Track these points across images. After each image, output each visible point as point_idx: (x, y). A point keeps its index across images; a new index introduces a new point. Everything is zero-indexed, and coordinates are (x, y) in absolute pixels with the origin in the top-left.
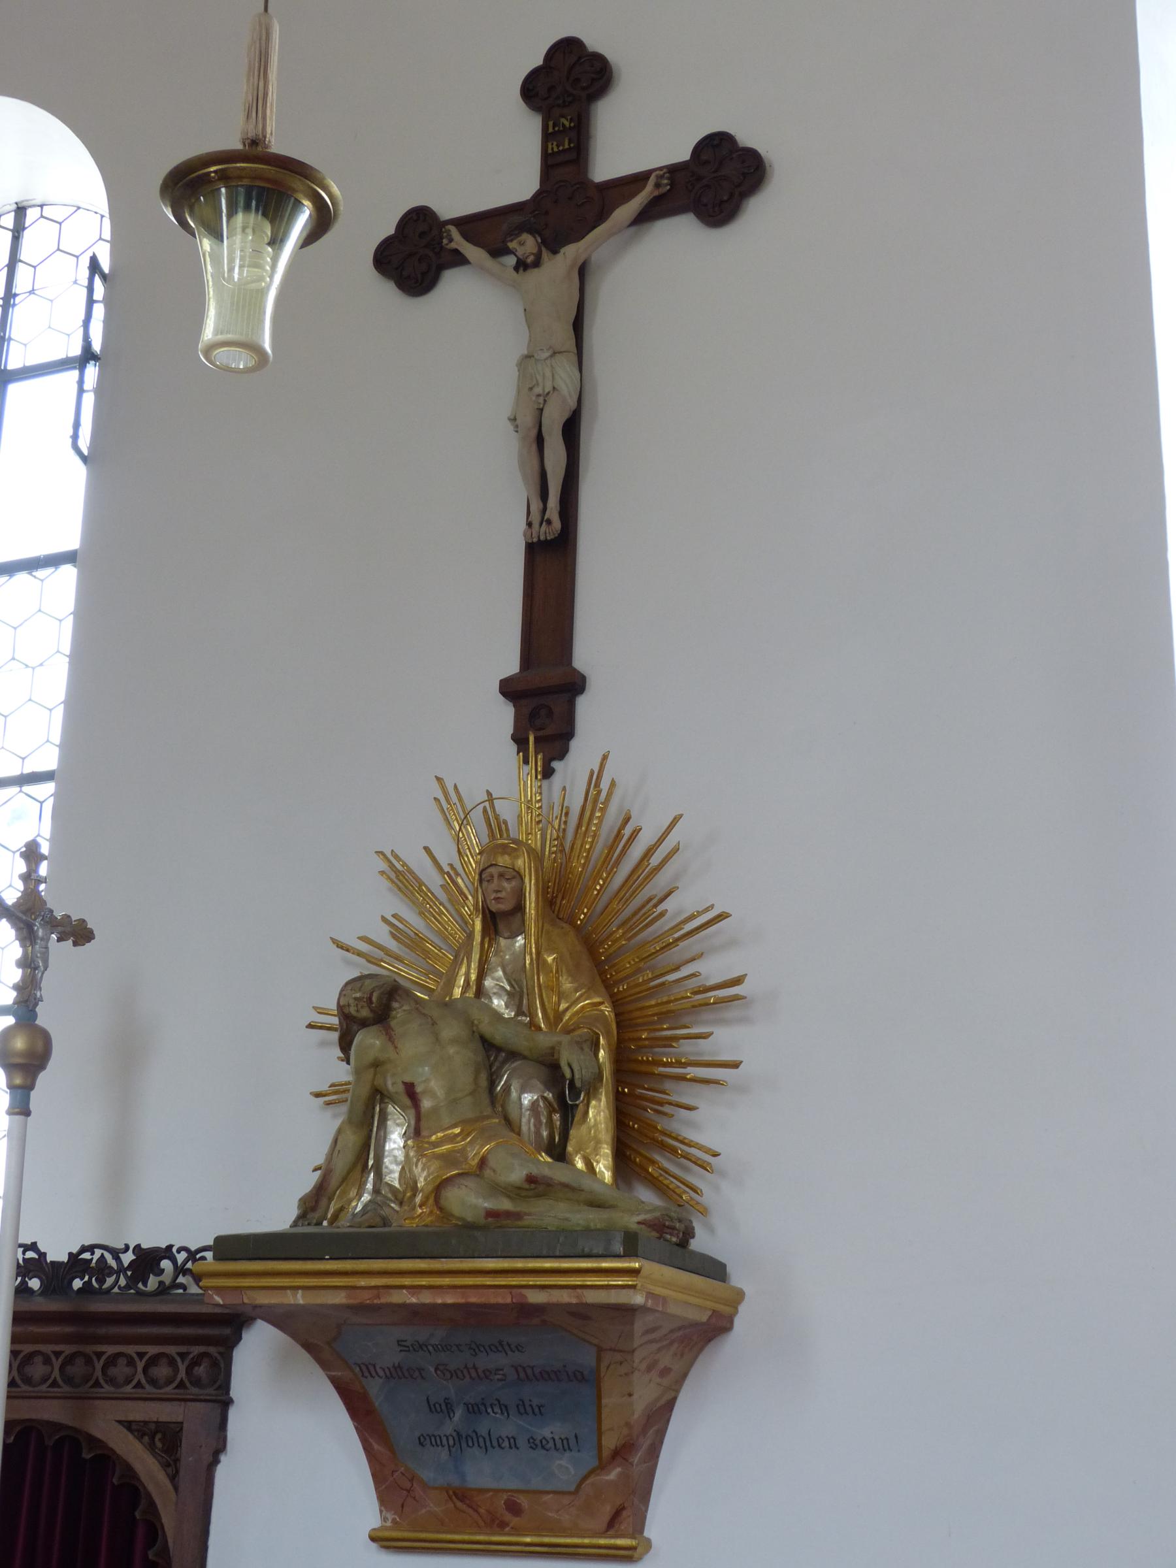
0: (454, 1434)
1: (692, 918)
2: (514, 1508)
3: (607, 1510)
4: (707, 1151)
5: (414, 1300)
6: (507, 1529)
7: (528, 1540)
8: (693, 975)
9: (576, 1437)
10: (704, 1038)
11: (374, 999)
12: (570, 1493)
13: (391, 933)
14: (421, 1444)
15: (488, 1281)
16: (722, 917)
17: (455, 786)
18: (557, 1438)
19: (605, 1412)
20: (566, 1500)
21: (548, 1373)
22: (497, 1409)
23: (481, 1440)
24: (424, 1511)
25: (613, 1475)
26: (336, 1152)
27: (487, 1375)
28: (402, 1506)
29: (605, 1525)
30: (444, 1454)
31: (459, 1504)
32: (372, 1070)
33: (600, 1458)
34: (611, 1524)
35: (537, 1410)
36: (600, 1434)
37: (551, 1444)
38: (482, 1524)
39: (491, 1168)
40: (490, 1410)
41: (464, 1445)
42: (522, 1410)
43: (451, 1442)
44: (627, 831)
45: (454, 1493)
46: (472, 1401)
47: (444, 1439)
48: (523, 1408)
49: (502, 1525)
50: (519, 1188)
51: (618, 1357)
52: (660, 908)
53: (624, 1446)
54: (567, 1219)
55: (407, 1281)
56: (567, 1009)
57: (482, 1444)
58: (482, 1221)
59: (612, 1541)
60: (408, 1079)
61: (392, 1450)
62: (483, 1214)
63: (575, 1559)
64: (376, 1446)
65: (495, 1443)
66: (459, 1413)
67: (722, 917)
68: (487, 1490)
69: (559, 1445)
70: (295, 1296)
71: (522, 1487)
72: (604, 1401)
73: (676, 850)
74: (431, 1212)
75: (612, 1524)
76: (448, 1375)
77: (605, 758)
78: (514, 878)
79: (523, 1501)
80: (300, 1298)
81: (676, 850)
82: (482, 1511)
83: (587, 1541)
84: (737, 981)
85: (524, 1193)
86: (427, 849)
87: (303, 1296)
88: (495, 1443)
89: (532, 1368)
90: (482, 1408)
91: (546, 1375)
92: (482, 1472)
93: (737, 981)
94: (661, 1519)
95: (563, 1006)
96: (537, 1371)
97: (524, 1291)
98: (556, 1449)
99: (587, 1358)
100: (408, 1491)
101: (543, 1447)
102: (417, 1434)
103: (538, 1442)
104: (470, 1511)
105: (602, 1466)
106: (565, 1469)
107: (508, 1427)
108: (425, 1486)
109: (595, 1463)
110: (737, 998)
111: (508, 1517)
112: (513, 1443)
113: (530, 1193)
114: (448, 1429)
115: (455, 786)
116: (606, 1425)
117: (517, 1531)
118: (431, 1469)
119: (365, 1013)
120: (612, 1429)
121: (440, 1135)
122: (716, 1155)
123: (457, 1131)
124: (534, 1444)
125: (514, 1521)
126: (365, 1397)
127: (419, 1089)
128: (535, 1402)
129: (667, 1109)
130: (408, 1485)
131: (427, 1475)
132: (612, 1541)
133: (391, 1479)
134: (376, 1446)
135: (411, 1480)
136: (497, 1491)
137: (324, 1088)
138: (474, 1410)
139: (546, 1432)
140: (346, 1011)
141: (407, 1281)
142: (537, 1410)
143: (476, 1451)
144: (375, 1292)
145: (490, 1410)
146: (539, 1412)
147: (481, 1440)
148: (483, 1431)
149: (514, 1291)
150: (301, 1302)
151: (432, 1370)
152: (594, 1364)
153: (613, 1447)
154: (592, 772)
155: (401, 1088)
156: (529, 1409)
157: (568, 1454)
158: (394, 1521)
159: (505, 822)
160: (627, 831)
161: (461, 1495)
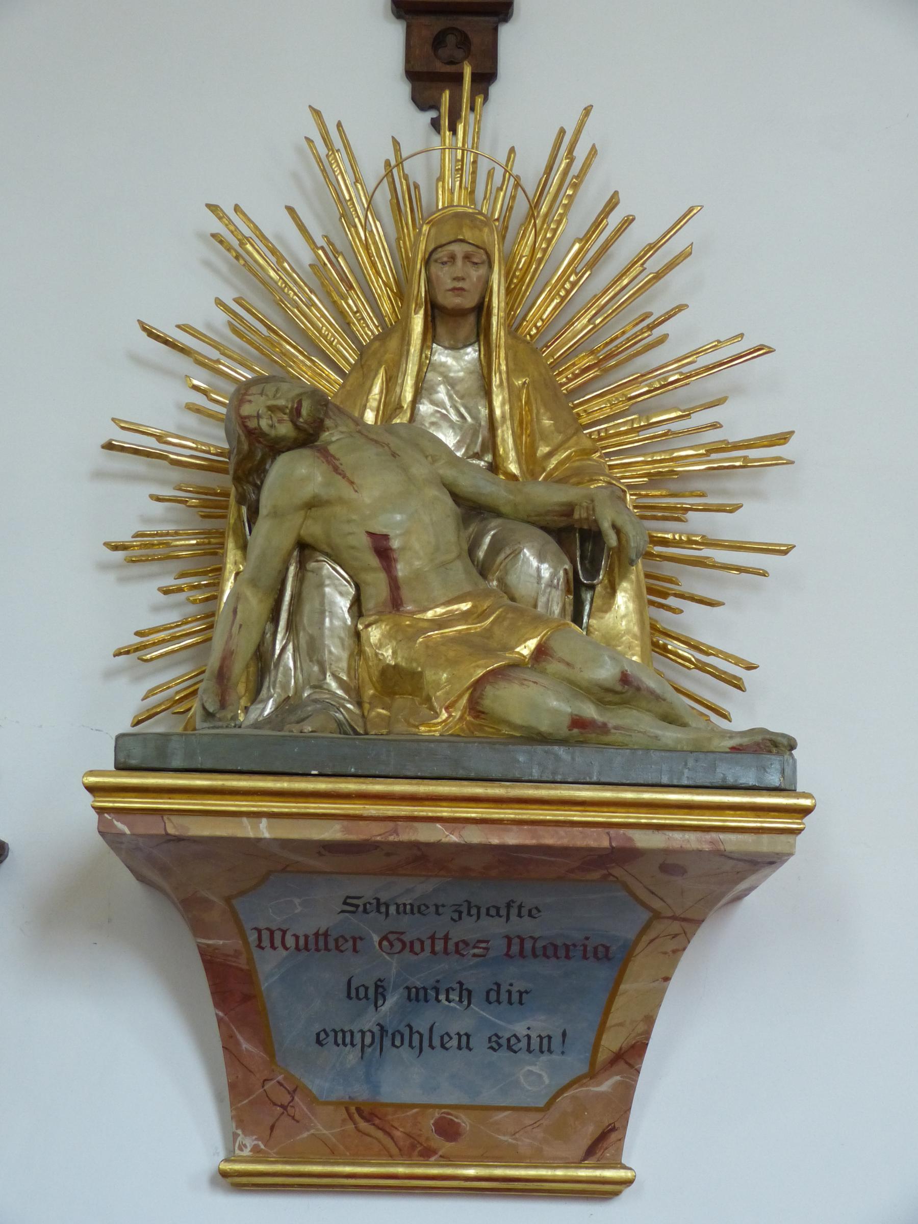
0: (376, 1029)
1: (718, 345)
2: (448, 1130)
3: (590, 1131)
4: (738, 661)
5: (454, 838)
6: (433, 1159)
7: (471, 1172)
8: (715, 426)
9: (564, 1034)
10: (731, 512)
11: (304, 412)
12: (537, 1110)
13: (230, 324)
14: (319, 1042)
15: (576, 816)
16: (762, 350)
17: (339, 125)
18: (534, 1035)
19: (619, 1001)
20: (528, 1119)
21: (556, 947)
22: (454, 996)
23: (416, 1037)
24: (305, 1135)
25: (606, 1086)
26: (236, 626)
27: (460, 948)
28: (272, 1128)
29: (581, 1152)
30: (352, 1056)
31: (363, 1125)
32: (302, 513)
33: (592, 1063)
34: (590, 1152)
35: (515, 997)
36: (602, 1028)
37: (524, 1044)
38: (394, 1150)
39: (561, 660)
40: (442, 997)
41: (387, 1042)
42: (493, 996)
43: (368, 1040)
44: (614, 220)
45: (358, 1110)
46: (419, 984)
47: (358, 1037)
48: (495, 995)
49: (427, 1154)
50: (608, 690)
51: (675, 927)
52: (658, 332)
53: (633, 1047)
54: (656, 737)
55: (445, 812)
56: (550, 455)
57: (416, 1042)
58: (564, 732)
59: (598, 1173)
60: (379, 529)
61: (272, 1055)
62: (566, 721)
63: (587, 1199)
64: (245, 1045)
65: (436, 1042)
66: (392, 1000)
67: (762, 350)
68: (413, 1106)
69: (535, 1042)
70: (256, 827)
71: (465, 1101)
72: (623, 987)
73: (685, 255)
74: (462, 718)
75: (590, 1152)
76: (398, 946)
77: (588, 111)
78: (483, 263)
79: (464, 1121)
80: (265, 830)
81: (685, 255)
82: (397, 1134)
83: (560, 1173)
84: (783, 438)
85: (610, 697)
86: (291, 210)
87: (269, 827)
88: (436, 1042)
89: (535, 939)
90: (432, 993)
91: (554, 951)
92: (405, 1081)
93: (783, 438)
94: (646, 1140)
95: (544, 449)
96: (540, 944)
97: (630, 833)
98: (529, 1050)
99: (623, 928)
100: (284, 1107)
101: (510, 1048)
102: (317, 1028)
103: (503, 1042)
104: (380, 1134)
105: (593, 1074)
106: (535, 1077)
107: (459, 1020)
108: (313, 1100)
109: (584, 1069)
110: (778, 462)
111: (437, 1141)
112: (465, 1042)
113: (616, 698)
114: (369, 1021)
115: (339, 125)
116: (612, 1020)
117: (447, 1160)
118: (329, 1078)
119: (285, 429)
120: (621, 1024)
121: (440, 610)
122: (750, 667)
123: (465, 606)
124: (496, 1043)
125: (446, 1147)
126: (249, 976)
127: (395, 544)
128: (519, 986)
129: (671, 601)
130: (286, 1099)
131: (317, 1084)
132: (598, 1173)
133: (262, 1090)
134: (245, 1045)
135: (292, 1093)
136: (425, 1107)
137: (125, 536)
138: (417, 996)
139: (520, 1029)
140: (252, 424)
141: (445, 812)
142: (515, 997)
143: (405, 1053)
144: (391, 825)
145: (442, 997)
146: (520, 1000)
147: (416, 1037)
148: (422, 1025)
149: (612, 832)
150: (267, 835)
151: (376, 938)
152: (631, 936)
153: (615, 1047)
154: (562, 132)
155: (365, 541)
156: (504, 997)
157: (544, 1058)
158: (255, 1149)
159: (416, 187)
160: (614, 220)
161: (370, 1113)
